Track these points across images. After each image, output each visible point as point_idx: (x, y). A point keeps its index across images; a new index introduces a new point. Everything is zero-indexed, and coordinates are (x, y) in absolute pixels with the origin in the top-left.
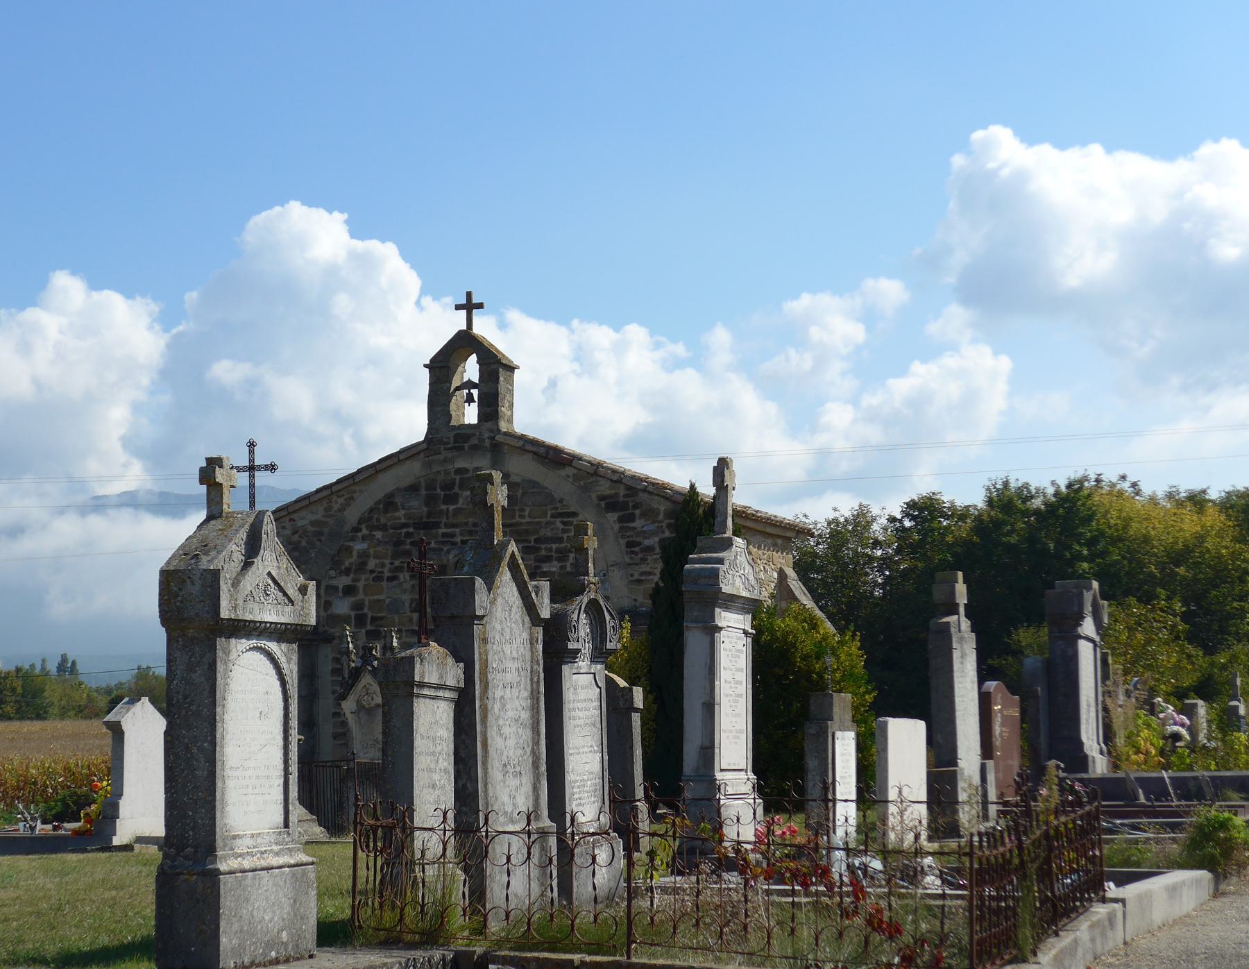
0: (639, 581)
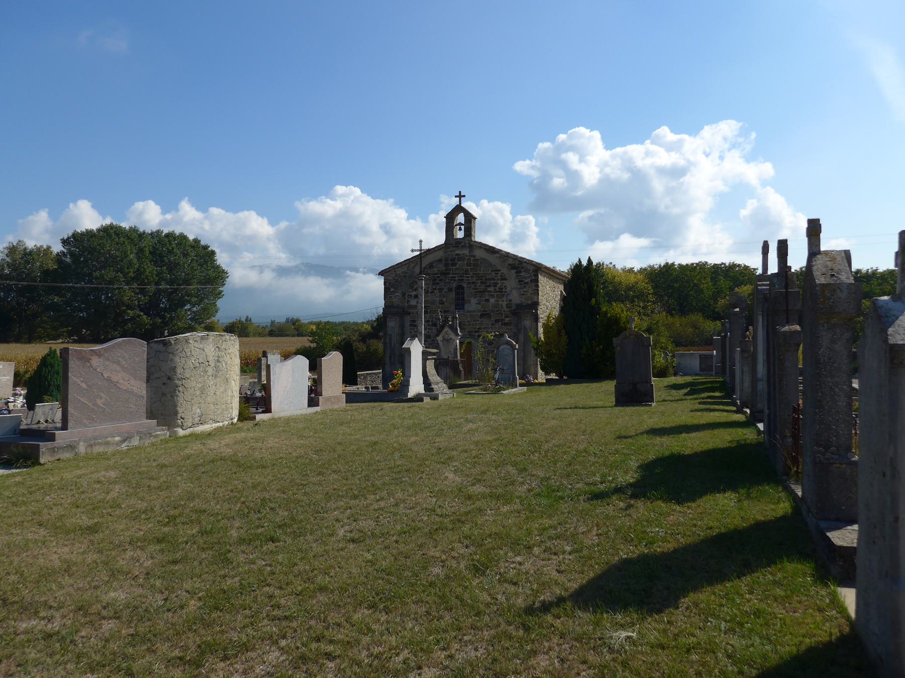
0: (523, 294)
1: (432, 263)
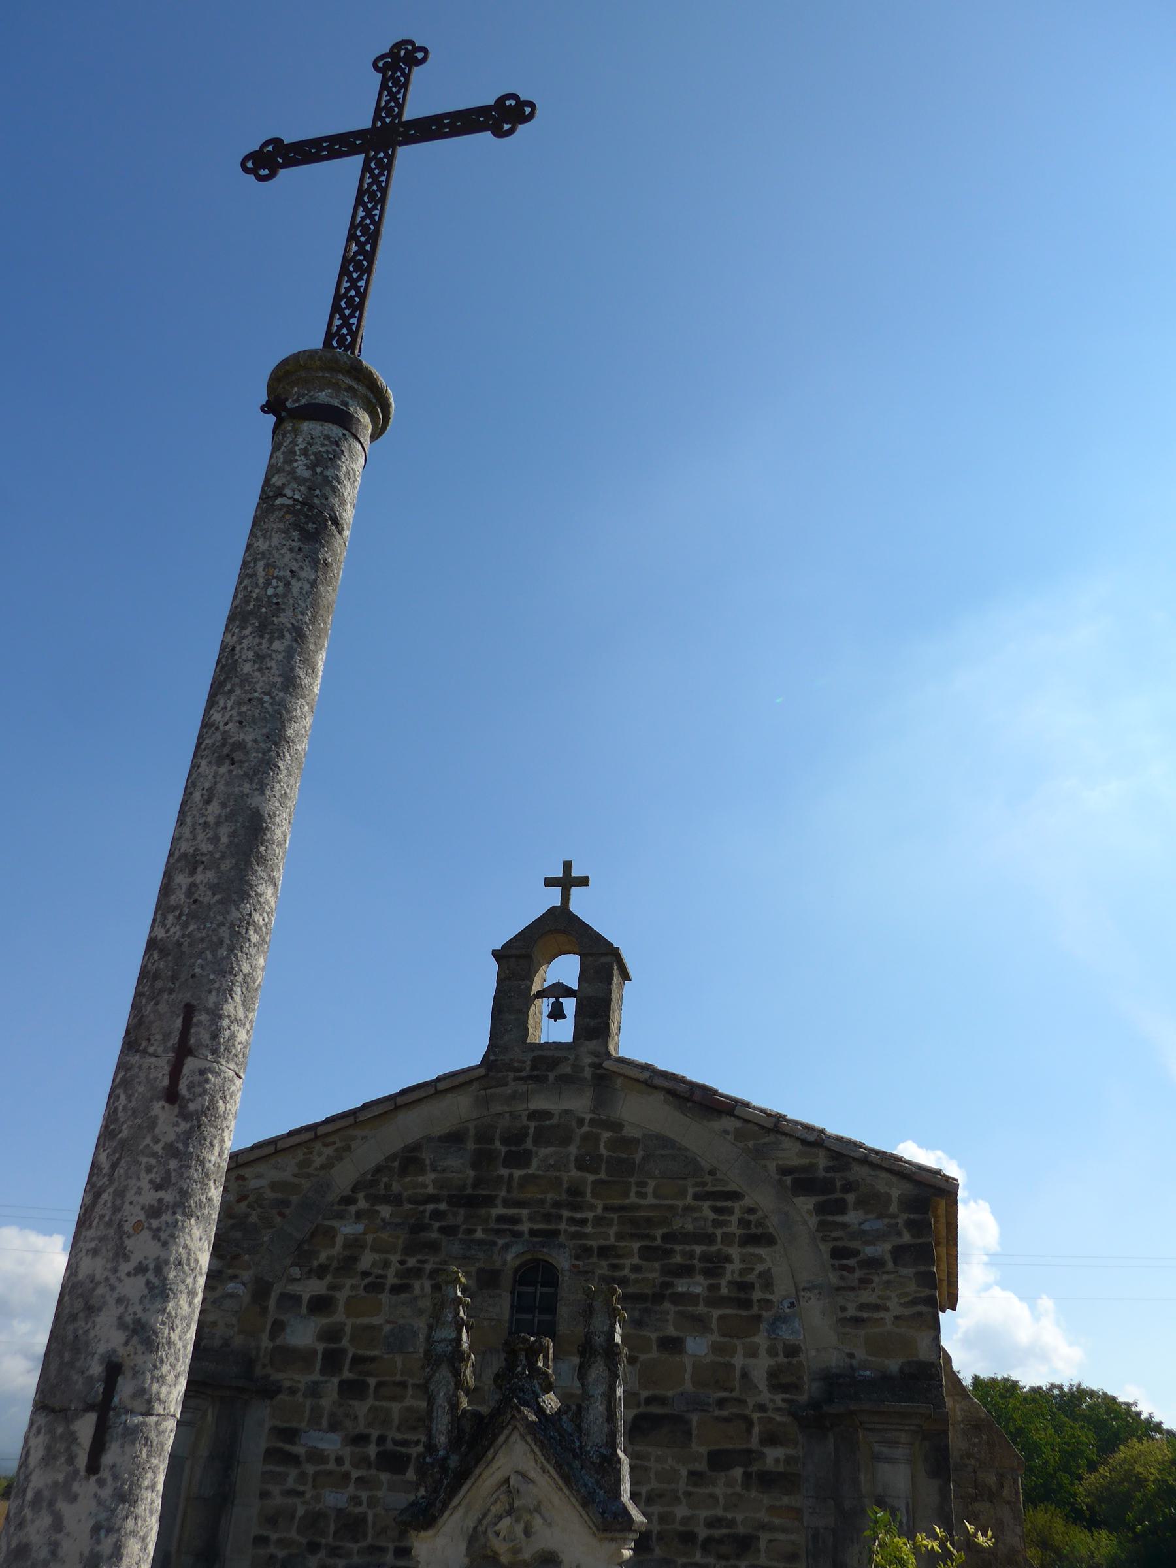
1: (416, 1147)
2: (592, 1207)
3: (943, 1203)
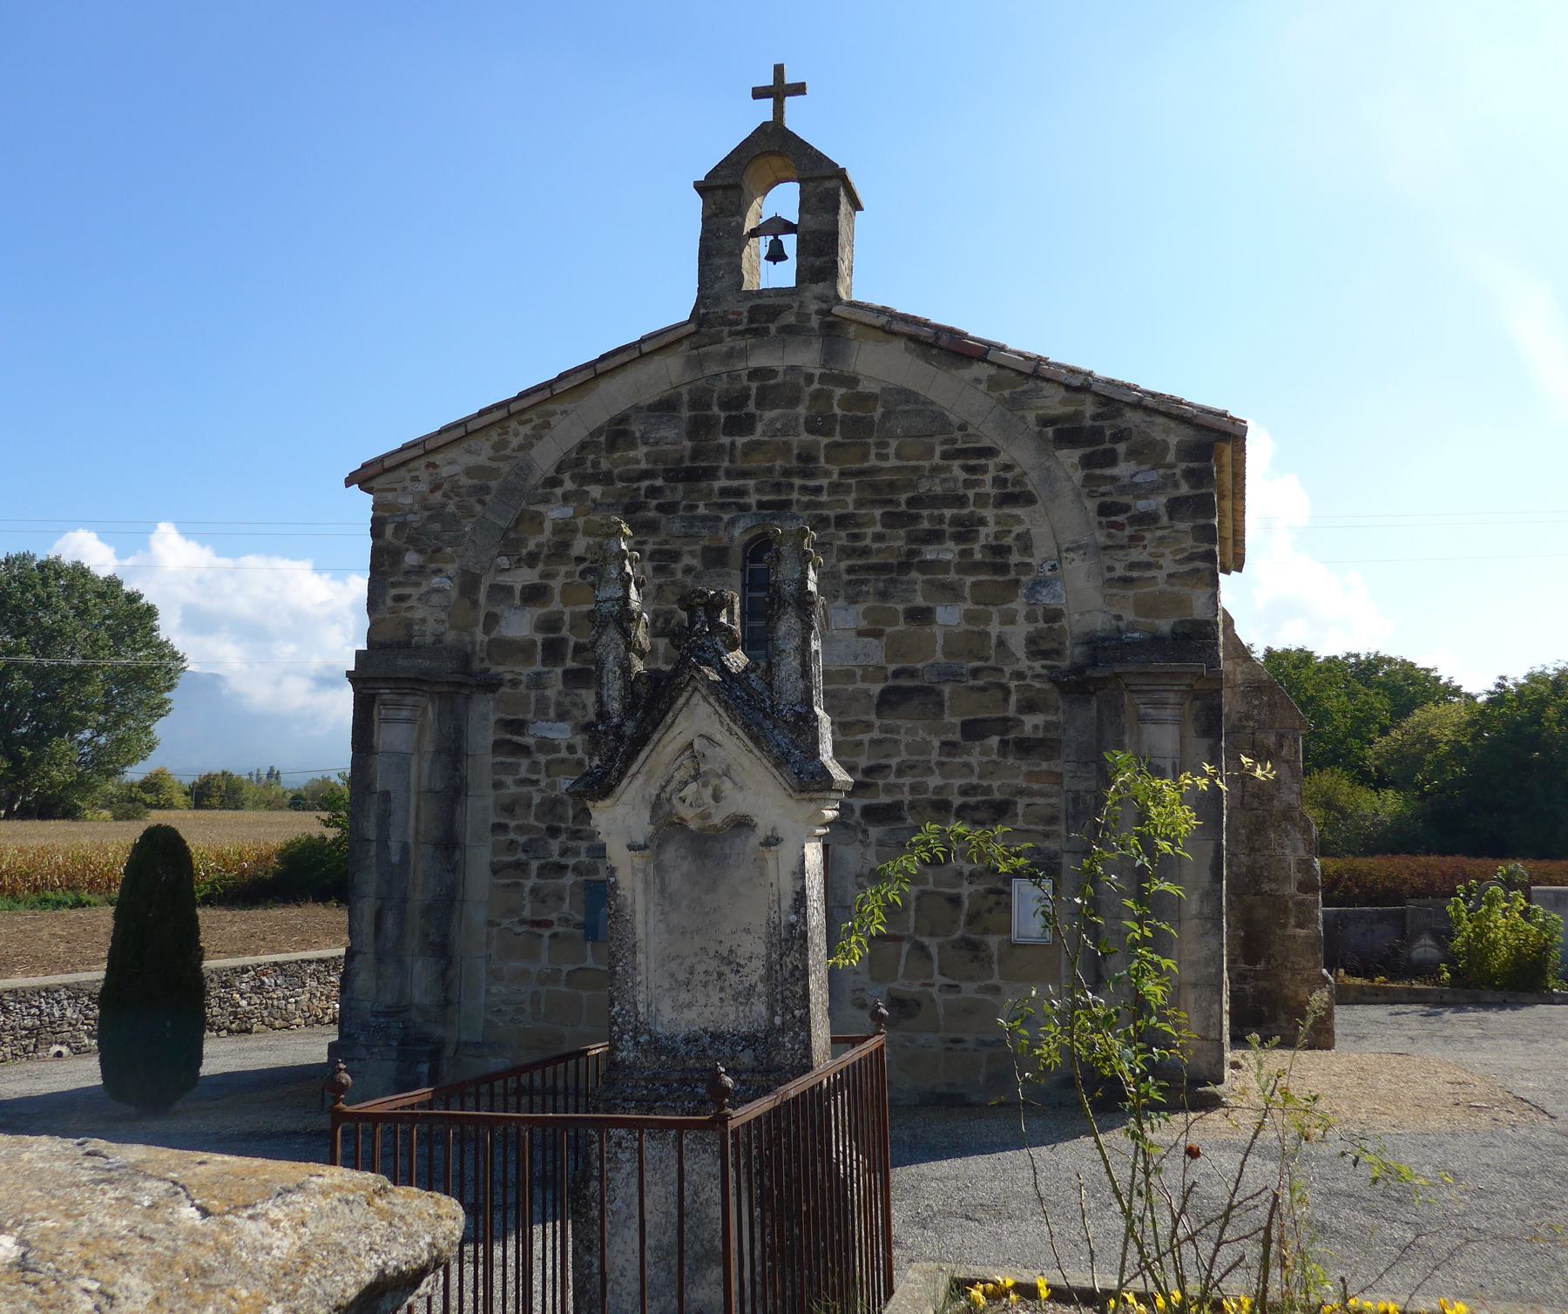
1: (623, 419)
2: (827, 473)
3: (1228, 450)
